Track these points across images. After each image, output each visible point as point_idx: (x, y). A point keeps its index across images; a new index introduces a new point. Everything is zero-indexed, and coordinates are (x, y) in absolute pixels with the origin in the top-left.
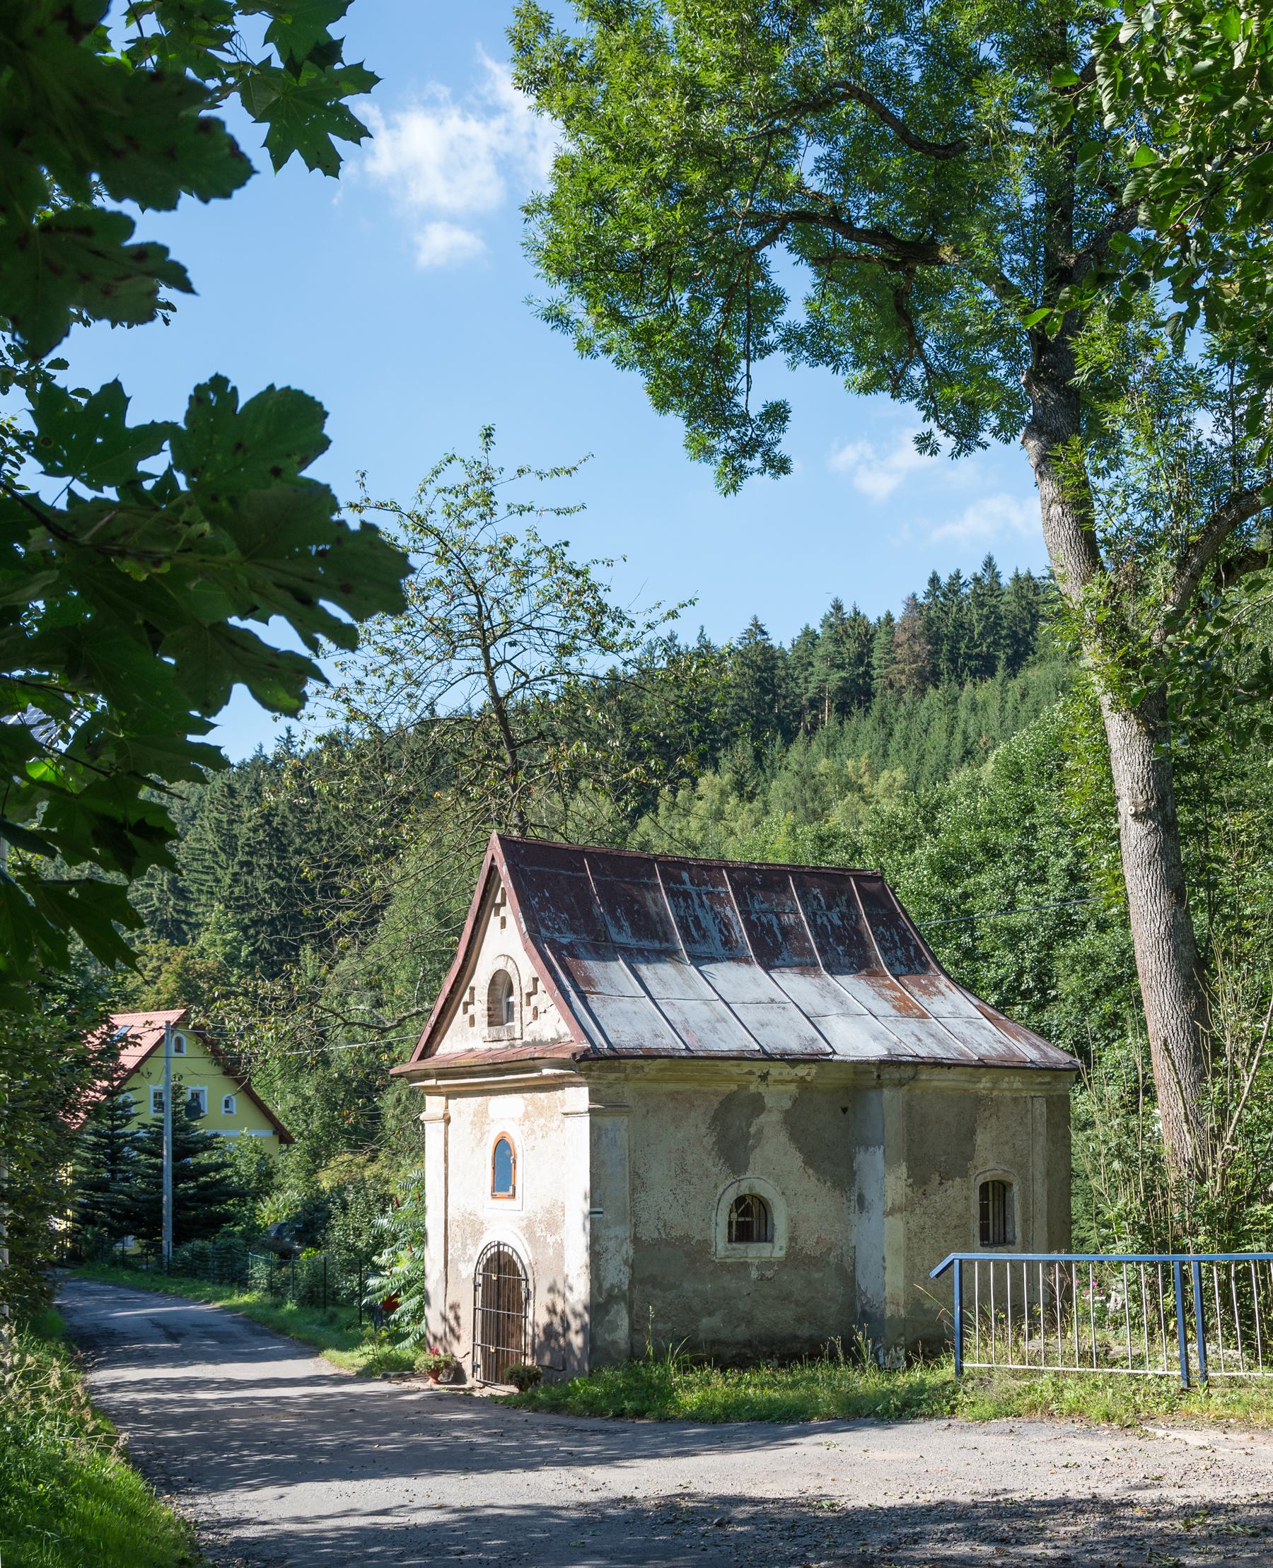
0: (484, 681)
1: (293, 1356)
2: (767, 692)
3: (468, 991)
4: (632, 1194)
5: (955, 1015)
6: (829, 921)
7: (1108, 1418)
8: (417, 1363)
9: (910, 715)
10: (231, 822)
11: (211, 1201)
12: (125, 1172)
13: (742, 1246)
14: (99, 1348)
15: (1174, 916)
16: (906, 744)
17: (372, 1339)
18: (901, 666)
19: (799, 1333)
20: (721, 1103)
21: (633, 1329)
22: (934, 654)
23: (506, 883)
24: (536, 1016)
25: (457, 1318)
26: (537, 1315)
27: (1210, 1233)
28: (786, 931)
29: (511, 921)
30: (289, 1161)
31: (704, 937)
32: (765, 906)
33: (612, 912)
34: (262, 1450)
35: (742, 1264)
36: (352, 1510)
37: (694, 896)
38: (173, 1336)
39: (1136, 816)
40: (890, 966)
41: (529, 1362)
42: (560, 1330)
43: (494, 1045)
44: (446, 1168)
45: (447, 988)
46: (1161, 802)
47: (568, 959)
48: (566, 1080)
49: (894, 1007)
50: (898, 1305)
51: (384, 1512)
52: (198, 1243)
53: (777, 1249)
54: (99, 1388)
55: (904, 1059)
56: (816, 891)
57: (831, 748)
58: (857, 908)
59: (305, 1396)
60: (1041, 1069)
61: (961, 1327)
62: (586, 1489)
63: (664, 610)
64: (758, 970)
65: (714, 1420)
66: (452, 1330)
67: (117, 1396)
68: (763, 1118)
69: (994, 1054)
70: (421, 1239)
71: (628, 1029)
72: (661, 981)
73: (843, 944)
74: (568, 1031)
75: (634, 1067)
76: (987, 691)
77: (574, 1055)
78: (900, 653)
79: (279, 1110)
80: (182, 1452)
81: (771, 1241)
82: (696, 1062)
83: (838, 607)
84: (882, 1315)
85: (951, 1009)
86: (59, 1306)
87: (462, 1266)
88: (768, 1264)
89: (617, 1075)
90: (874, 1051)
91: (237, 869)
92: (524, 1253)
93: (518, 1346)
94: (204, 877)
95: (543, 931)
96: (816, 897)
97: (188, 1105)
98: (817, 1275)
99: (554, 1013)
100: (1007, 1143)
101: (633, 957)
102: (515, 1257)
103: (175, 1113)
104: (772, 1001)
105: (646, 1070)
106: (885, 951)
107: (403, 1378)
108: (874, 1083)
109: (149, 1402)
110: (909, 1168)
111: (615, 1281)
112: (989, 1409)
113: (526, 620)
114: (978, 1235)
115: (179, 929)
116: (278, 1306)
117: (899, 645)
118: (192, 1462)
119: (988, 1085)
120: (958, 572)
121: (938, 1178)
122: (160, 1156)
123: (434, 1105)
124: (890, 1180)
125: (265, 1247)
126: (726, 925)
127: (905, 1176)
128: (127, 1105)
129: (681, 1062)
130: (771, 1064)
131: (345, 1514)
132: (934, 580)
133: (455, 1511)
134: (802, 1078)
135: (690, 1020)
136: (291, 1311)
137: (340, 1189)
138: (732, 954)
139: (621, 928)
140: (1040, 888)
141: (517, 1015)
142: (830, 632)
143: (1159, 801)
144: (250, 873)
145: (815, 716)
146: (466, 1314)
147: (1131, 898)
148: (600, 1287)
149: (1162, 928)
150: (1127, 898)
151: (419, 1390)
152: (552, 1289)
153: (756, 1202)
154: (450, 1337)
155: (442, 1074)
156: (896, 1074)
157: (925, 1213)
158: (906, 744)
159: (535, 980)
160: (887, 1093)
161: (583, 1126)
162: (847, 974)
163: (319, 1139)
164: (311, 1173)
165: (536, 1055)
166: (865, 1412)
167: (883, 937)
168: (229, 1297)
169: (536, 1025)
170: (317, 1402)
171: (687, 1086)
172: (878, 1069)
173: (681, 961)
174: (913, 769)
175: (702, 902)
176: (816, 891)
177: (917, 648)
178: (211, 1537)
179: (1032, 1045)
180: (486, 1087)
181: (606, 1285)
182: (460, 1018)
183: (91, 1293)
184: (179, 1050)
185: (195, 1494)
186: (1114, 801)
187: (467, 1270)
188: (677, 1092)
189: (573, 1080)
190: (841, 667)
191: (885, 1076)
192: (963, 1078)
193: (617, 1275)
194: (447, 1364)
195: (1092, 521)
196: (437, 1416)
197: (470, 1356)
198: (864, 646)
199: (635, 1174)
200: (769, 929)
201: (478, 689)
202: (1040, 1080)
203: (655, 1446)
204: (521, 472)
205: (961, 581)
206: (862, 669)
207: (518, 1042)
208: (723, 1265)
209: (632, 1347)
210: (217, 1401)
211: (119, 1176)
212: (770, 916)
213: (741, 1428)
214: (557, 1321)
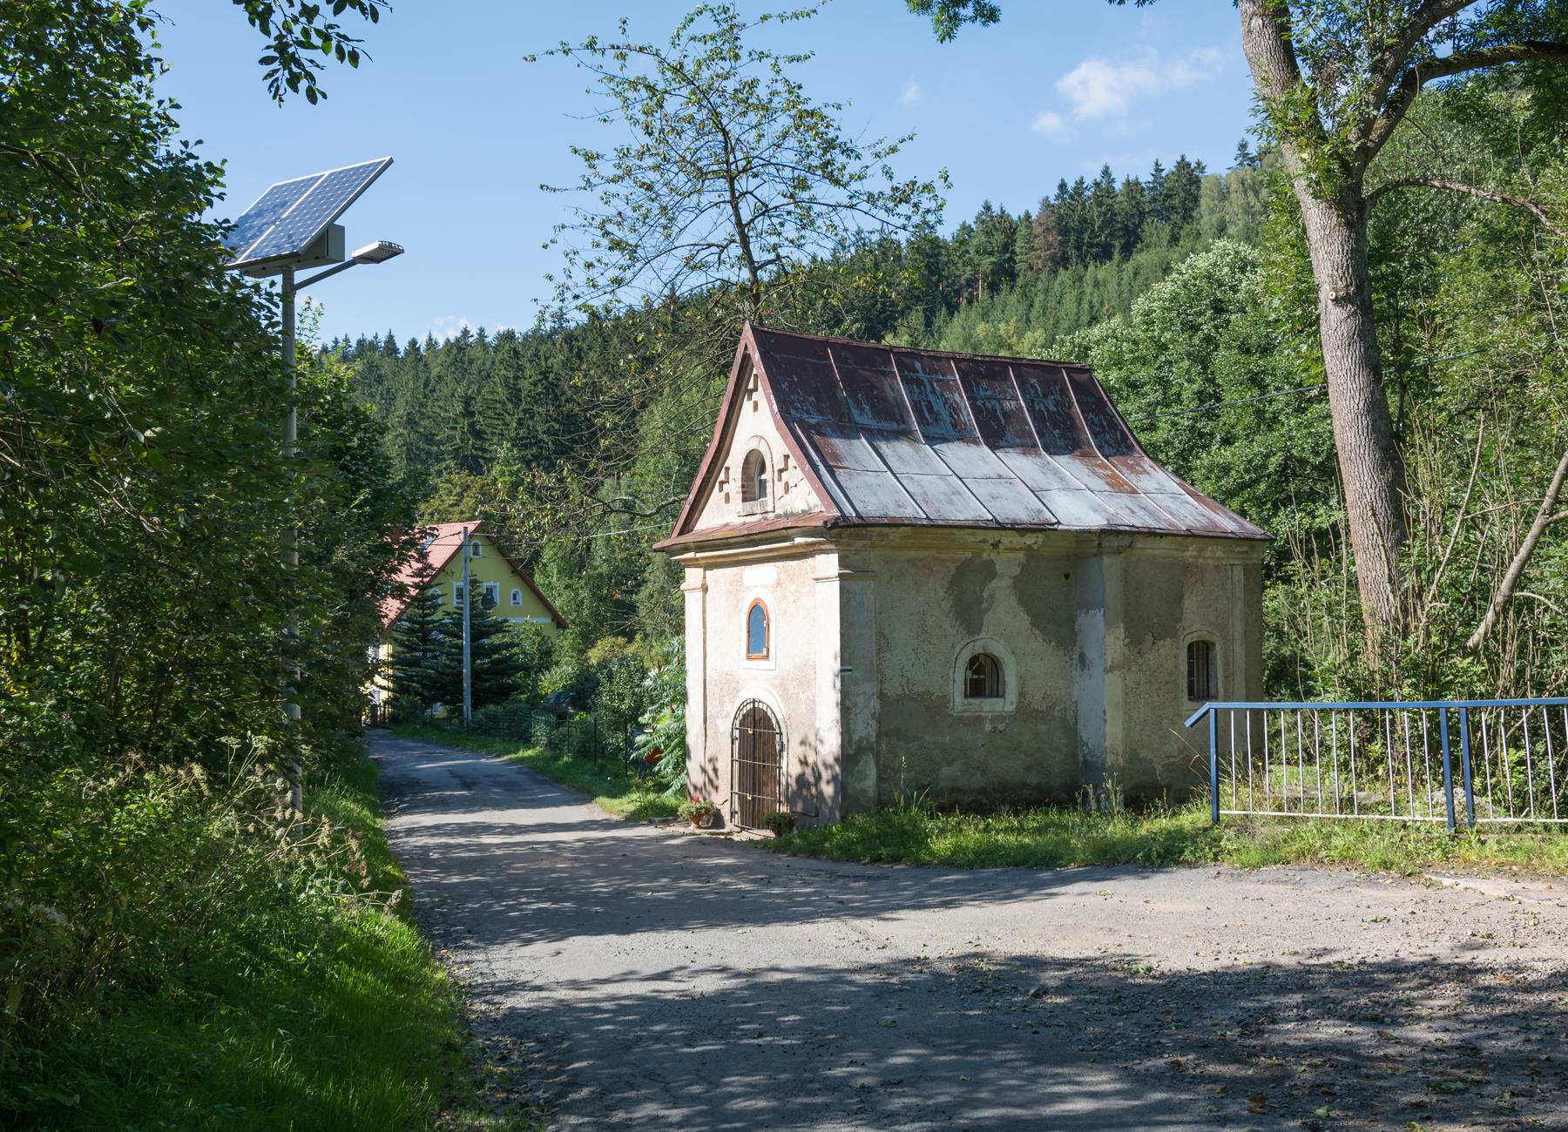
1: (568, 803)
2: (932, 273)
4: (878, 654)
5: (1161, 491)
7: (1386, 865)
8: (680, 810)
9: (1047, 291)
10: (516, 378)
11: (502, 673)
12: (434, 651)
13: (976, 701)
14: (405, 795)
15: (1372, 393)
16: (1044, 313)
17: (638, 787)
19: (1028, 781)
21: (880, 778)
22: (1063, 243)
23: (759, 369)
24: (787, 490)
25: (715, 770)
26: (790, 766)
27: (1414, 686)
29: (763, 404)
30: (565, 642)
31: (936, 419)
32: (989, 393)
34: (539, 897)
36: (632, 973)
37: (927, 383)
38: (466, 785)
39: (1336, 301)
40: (1100, 448)
41: (784, 809)
42: (812, 779)
43: (749, 519)
44: (705, 633)
47: (816, 437)
48: (817, 547)
49: (1107, 483)
51: (664, 976)
52: (491, 707)
53: (1008, 703)
54: (398, 832)
55: (1122, 528)
56: (1033, 381)
57: (985, 316)
58: (1069, 396)
59: (579, 840)
61: (1218, 776)
62: (873, 948)
63: (886, 146)
64: (985, 450)
65: (970, 866)
66: (711, 781)
67: (412, 840)
68: (994, 583)
69: (1199, 525)
70: (682, 698)
71: (873, 500)
72: (901, 459)
74: (819, 502)
75: (880, 535)
76: (1105, 271)
77: (826, 522)
78: (1037, 243)
79: (557, 604)
80: (466, 898)
81: (1003, 696)
82: (935, 531)
83: (988, 208)
84: (1104, 764)
86: (375, 760)
87: (719, 722)
88: (1000, 718)
90: (1095, 521)
91: (521, 415)
92: (777, 708)
93: (773, 793)
94: (496, 422)
95: (793, 412)
96: (1033, 386)
97: (484, 596)
98: (1044, 728)
99: (805, 486)
101: (873, 435)
102: (769, 713)
103: (472, 603)
104: (1000, 477)
105: (891, 537)
106: (1094, 434)
107: (666, 823)
108: (1095, 551)
109: (438, 846)
111: (864, 734)
112: (1255, 857)
113: (766, 155)
114: (1186, 690)
115: (477, 463)
116: (556, 759)
117: (1036, 236)
118: (472, 911)
122: (461, 638)
123: (693, 576)
124: (1110, 639)
125: (546, 710)
126: (955, 410)
127: (1122, 636)
128: (435, 597)
129: (925, 530)
130: (1003, 533)
131: (624, 978)
132: (1063, 186)
133: (738, 975)
134: (1030, 546)
137: (603, 664)
138: (959, 434)
140: (1175, 409)
141: (769, 490)
142: (981, 227)
143: (1357, 287)
144: (532, 418)
145: (971, 293)
146: (724, 765)
147: (1331, 378)
148: (850, 740)
149: (1361, 404)
150: (1326, 376)
151: (683, 835)
152: (803, 743)
153: (989, 661)
154: (709, 787)
155: (701, 546)
156: (1114, 542)
158: (1044, 313)
159: (787, 457)
160: (1106, 560)
161: (833, 589)
163: (588, 625)
164: (582, 652)
166: (1123, 858)
169: (787, 497)
170: (589, 847)
171: (926, 554)
172: (1099, 537)
173: (916, 441)
174: (1050, 332)
177: (1050, 239)
178: (483, 1007)
179: (1230, 518)
181: (856, 738)
182: (716, 496)
183: (404, 749)
184: (476, 553)
185: (473, 948)
186: (1315, 289)
187: (724, 725)
190: (991, 254)
191: (1105, 544)
192: (1173, 546)
193: (866, 729)
194: (707, 811)
195: (1289, 29)
196: (701, 861)
197: (729, 803)
198: (1009, 237)
199: (881, 634)
201: (722, 219)
202: (1239, 549)
203: (921, 894)
204: (765, 18)
206: (1007, 255)
207: (771, 516)
208: (960, 718)
209: (879, 795)
210: (498, 846)
211: (429, 654)
212: (994, 402)
213: (997, 874)
214: (808, 771)
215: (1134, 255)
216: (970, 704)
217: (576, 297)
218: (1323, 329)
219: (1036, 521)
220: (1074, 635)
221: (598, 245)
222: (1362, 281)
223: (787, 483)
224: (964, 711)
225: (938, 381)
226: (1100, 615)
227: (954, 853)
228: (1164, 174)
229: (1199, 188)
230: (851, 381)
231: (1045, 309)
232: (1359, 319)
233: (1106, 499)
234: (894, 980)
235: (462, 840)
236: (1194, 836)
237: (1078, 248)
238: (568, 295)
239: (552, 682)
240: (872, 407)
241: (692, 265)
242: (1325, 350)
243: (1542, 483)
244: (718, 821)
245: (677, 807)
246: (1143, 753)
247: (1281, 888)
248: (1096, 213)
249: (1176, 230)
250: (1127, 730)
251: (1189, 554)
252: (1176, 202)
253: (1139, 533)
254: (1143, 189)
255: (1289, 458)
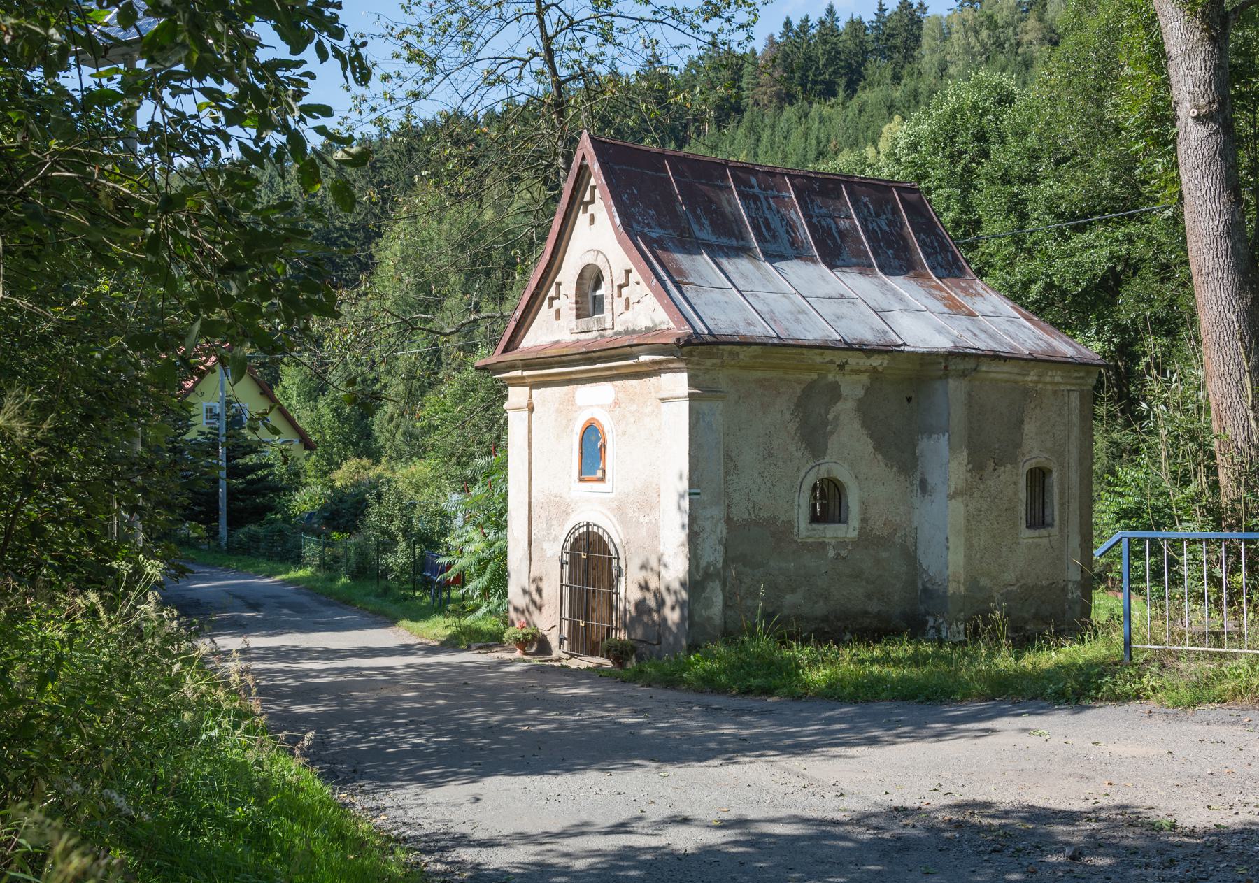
0: (536, 21)
3: (554, 286)
4: (725, 477)
6: (879, 227)
8: (506, 635)
9: (773, 127)
11: (257, 493)
13: (820, 527)
15: (1233, 214)
18: (764, 88)
19: (870, 609)
20: (803, 391)
21: (726, 606)
23: (597, 178)
24: (627, 306)
25: (539, 591)
26: (628, 592)
28: (842, 233)
31: (774, 236)
32: (824, 211)
33: (693, 211)
35: (821, 543)
37: (763, 199)
39: (1198, 119)
40: (933, 269)
41: (622, 635)
44: (530, 454)
45: (533, 284)
46: (1222, 105)
47: (659, 252)
49: (945, 305)
50: (959, 582)
51: (621, 828)
52: (252, 527)
53: (851, 530)
56: (866, 199)
58: (900, 216)
59: (408, 666)
60: (1080, 364)
64: (824, 269)
65: (853, 699)
66: (534, 602)
68: (839, 406)
69: (1039, 349)
71: (723, 317)
72: (743, 275)
73: (892, 248)
75: (730, 353)
77: (678, 340)
79: (302, 424)
81: (846, 522)
82: (785, 350)
84: (945, 592)
85: (992, 309)
87: (546, 546)
88: (842, 544)
89: (714, 361)
90: (942, 343)
92: (613, 531)
95: (635, 226)
96: (865, 205)
98: (885, 555)
100: (1048, 432)
101: (716, 252)
102: (605, 538)
104: (842, 296)
105: (741, 356)
106: (927, 255)
110: (969, 455)
116: (333, 580)
119: (1035, 378)
120: (807, 16)
121: (993, 464)
123: (517, 395)
124: (954, 465)
126: (791, 228)
127: (965, 462)
130: (850, 353)
132: (788, 24)
135: (776, 311)
136: (345, 585)
138: (797, 252)
139: (702, 225)
141: (607, 306)
143: (1220, 104)
147: (1187, 199)
149: (1221, 226)
152: (644, 567)
153: (832, 486)
154: (532, 608)
155: (528, 364)
156: (962, 365)
157: (981, 497)
160: (952, 383)
162: (898, 275)
165: (635, 342)
167: (925, 244)
168: (287, 572)
169: (628, 315)
173: (756, 258)
175: (770, 205)
176: (866, 199)
177: (776, 75)
180: (574, 376)
181: (703, 563)
182: (545, 312)
188: (767, 380)
189: (671, 366)
191: (952, 367)
192: (1016, 370)
193: (713, 555)
199: (728, 457)
200: (828, 232)
202: (1076, 374)
205: (810, 24)
207: (609, 333)
215: (859, 93)
216: (814, 530)
217: (373, 110)
218: (1181, 149)
219: (882, 342)
220: (915, 459)
221: (398, 56)
222: (1224, 99)
223: (627, 300)
224: (808, 537)
225: (774, 197)
226: (944, 440)
227: (830, 686)
228: (887, 14)
229: (920, 28)
230: (691, 195)
231: (772, 143)
232: (1220, 138)
233: (947, 322)
234: (887, 835)
235: (281, 665)
236: (1105, 668)
237: (803, 86)
238: (365, 106)
239: (305, 500)
240: (712, 223)
241: (492, 79)
242: (1182, 170)
243: (1151, 323)
244: (543, 647)
245: (503, 633)
246: (984, 581)
247: (1233, 729)
248: (821, 51)
249: (898, 69)
250: (968, 558)
251: (1029, 378)
252: (898, 41)
253: (985, 356)
254: (866, 28)
255: (1050, 286)
